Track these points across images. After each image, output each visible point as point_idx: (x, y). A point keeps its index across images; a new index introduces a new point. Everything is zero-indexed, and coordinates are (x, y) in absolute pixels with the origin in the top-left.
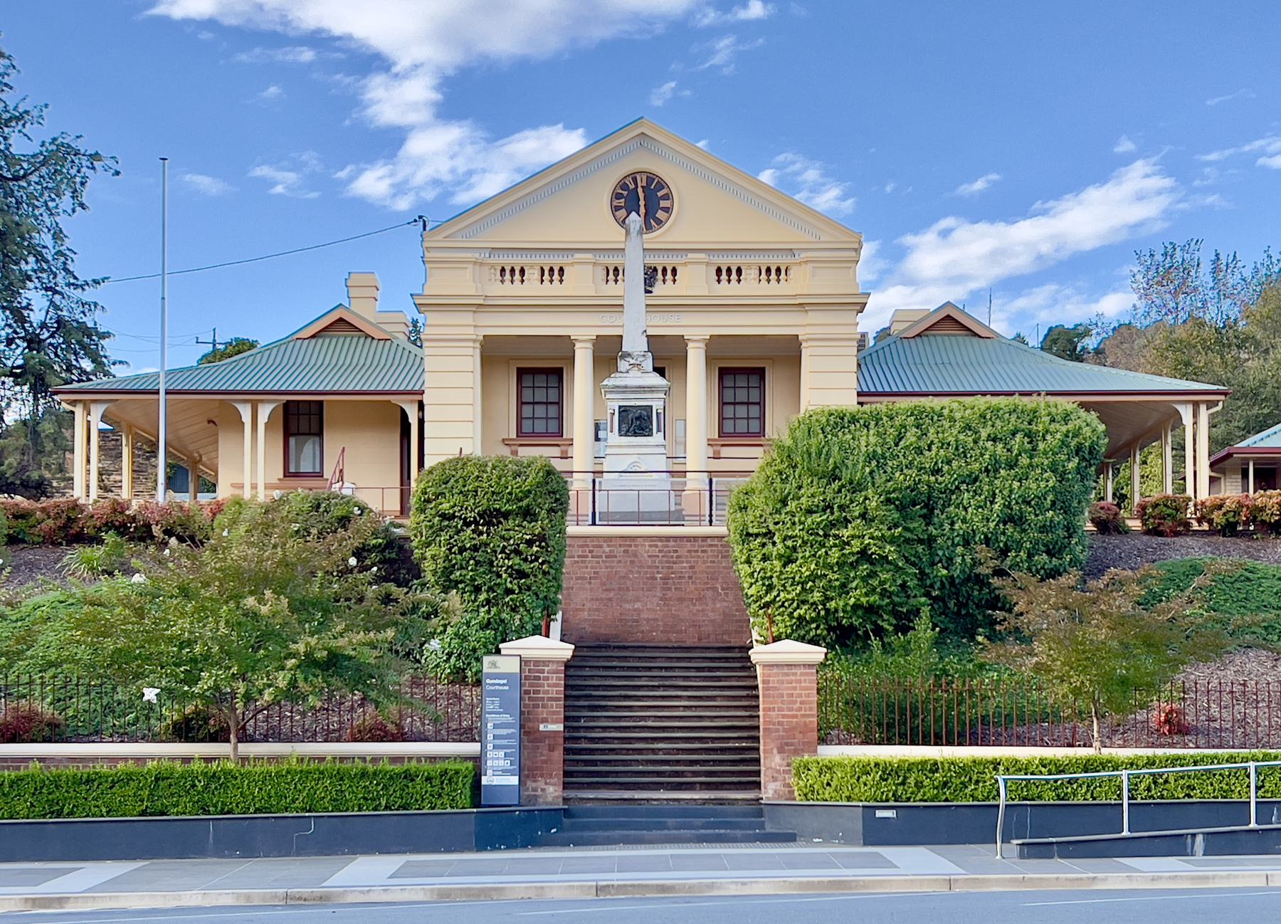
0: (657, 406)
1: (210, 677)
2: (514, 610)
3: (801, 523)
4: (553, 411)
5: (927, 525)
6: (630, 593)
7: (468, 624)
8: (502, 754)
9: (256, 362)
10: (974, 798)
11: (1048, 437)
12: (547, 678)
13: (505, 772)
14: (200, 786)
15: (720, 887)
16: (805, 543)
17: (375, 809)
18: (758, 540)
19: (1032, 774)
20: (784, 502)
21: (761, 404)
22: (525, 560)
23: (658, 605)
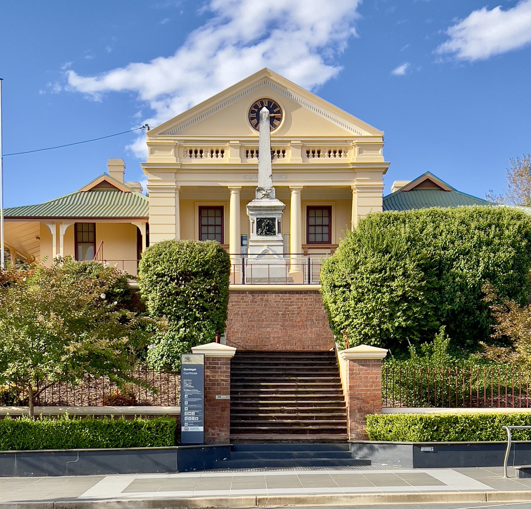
0: (278, 217)
1: (14, 366)
2: (200, 330)
3: (367, 278)
4: (218, 229)
5: (439, 279)
6: (265, 323)
7: (173, 338)
8: (193, 413)
9: (60, 203)
10: (481, 439)
11: (511, 228)
12: (220, 368)
13: (195, 424)
14: (9, 432)
15: (337, 499)
16: (369, 290)
17: (116, 447)
18: (341, 289)
19: (515, 424)
20: (356, 267)
21: (329, 226)
22: (206, 301)
23: (281, 329)
